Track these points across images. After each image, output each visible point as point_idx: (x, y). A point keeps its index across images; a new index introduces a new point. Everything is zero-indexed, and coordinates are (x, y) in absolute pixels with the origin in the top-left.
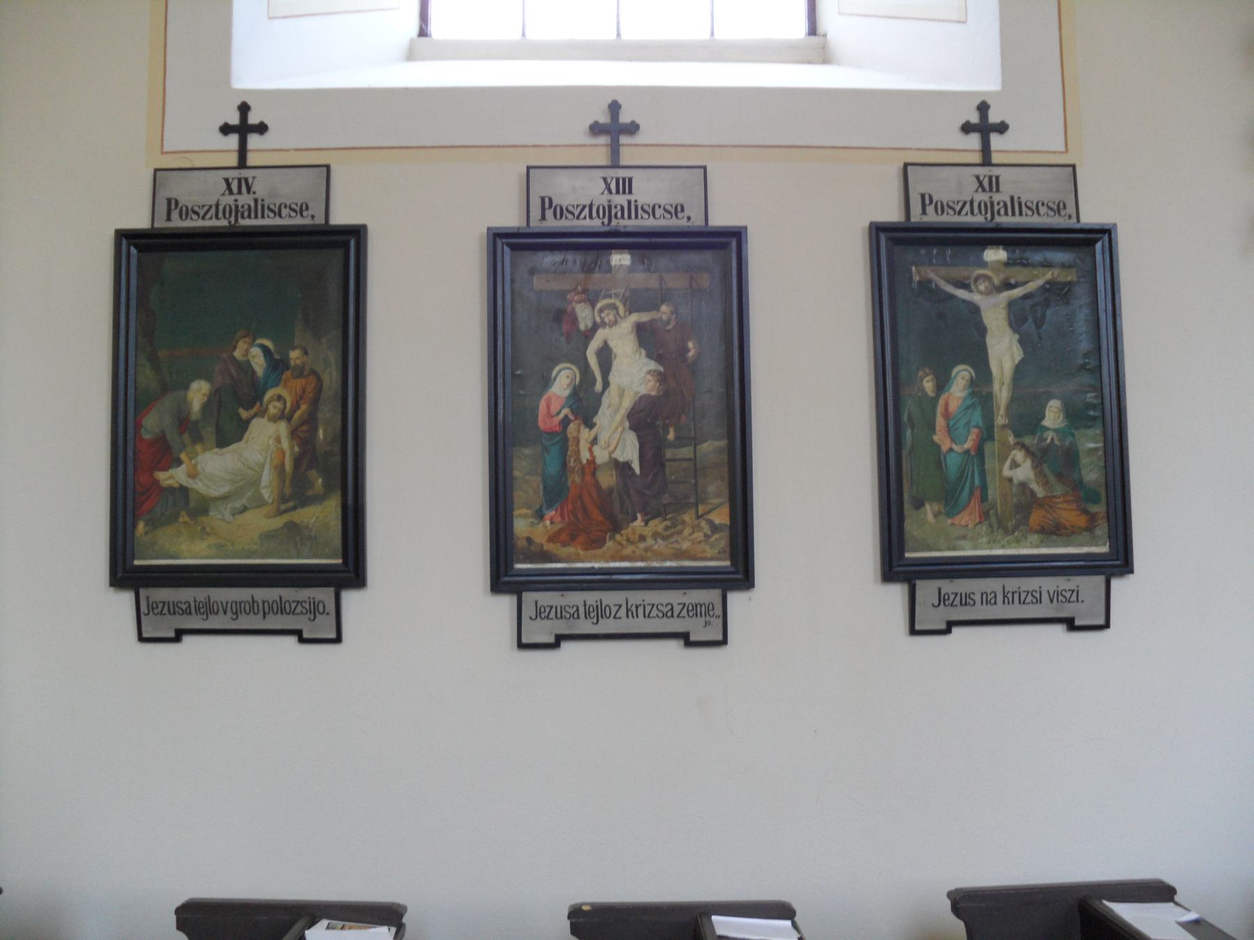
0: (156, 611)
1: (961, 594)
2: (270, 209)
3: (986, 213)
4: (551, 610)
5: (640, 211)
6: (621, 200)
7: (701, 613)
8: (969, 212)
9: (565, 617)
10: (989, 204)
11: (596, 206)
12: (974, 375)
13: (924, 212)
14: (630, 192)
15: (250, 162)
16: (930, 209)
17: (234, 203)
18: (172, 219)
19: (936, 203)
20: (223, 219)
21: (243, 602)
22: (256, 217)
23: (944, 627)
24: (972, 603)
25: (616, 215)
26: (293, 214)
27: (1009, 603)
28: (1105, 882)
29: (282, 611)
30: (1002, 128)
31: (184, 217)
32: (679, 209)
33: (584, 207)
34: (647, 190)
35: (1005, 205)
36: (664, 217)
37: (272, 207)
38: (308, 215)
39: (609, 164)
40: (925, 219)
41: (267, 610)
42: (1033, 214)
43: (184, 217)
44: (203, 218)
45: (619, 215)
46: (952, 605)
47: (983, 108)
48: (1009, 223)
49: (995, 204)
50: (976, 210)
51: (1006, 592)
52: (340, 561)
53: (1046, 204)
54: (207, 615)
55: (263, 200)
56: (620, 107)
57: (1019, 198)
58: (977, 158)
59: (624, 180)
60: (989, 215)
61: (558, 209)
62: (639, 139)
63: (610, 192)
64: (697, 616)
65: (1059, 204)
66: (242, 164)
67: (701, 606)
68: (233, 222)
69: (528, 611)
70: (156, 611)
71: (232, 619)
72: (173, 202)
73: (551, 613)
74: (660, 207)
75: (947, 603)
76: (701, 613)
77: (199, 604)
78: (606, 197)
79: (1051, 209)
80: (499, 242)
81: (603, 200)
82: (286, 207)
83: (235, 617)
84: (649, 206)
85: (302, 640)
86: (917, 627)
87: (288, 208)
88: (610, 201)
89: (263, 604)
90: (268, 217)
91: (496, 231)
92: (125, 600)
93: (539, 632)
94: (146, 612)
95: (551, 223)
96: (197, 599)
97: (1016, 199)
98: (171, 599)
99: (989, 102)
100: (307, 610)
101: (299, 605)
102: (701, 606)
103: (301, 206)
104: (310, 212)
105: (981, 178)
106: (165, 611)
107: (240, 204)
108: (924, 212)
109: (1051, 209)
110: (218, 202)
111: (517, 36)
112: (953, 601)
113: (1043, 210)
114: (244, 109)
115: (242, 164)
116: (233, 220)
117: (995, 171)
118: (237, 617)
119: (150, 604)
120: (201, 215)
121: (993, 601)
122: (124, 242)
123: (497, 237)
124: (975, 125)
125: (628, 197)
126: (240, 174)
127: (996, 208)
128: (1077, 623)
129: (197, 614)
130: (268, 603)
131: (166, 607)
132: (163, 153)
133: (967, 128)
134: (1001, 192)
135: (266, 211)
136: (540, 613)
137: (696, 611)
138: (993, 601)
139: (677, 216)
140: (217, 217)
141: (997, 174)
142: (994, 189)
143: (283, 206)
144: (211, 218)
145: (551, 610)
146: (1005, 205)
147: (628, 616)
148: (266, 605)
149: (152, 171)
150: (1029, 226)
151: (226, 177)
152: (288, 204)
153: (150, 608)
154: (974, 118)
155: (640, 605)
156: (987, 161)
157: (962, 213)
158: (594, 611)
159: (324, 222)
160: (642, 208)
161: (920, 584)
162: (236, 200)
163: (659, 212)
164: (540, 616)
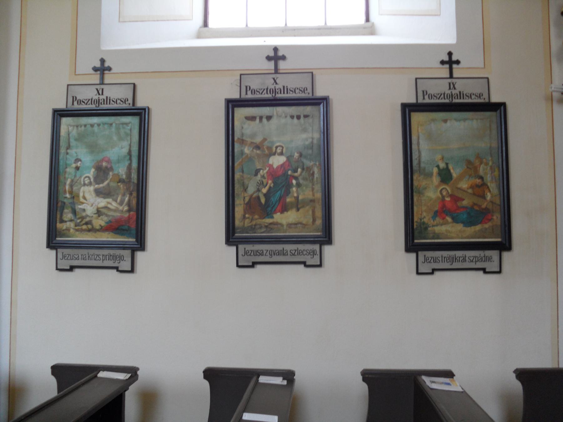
0: (66, 258)
1: (254, 251)
2: (113, 101)
4: (251, 252)
13: (424, 98)
16: (426, 97)
19: (429, 95)
20: (93, 105)
21: (446, 257)
22: (460, 98)
23: (431, 271)
24: (438, 261)
27: (458, 261)
29: (299, 254)
30: (284, 58)
34: (112, 93)
36: (299, 93)
42: (469, 98)
45: (103, 103)
46: (250, 255)
51: (456, 257)
54: (313, 256)
57: (110, 97)
58: (273, 72)
62: (460, 66)
63: (99, 94)
71: (270, 257)
72: (425, 92)
74: (119, 99)
75: (248, 254)
77: (299, 251)
78: (98, 96)
79: (300, 90)
81: (96, 97)
82: (473, 94)
83: (271, 256)
84: (123, 99)
85: (118, 271)
87: (474, 95)
88: (99, 97)
89: (280, 251)
96: (443, 256)
97: (461, 93)
101: (472, 260)
102: (476, 257)
105: (99, 90)
109: (477, 96)
110: (445, 92)
111: (322, 24)
112: (431, 260)
114: (103, 61)
117: (454, 81)
118: (272, 257)
121: (286, 254)
138: (286, 254)
144: (89, 104)
145: (251, 252)
146: (457, 95)
151: (97, 88)
152: (474, 94)
153: (426, 260)
157: (88, 104)
160: (466, 94)
161: (420, 253)
163: (297, 91)
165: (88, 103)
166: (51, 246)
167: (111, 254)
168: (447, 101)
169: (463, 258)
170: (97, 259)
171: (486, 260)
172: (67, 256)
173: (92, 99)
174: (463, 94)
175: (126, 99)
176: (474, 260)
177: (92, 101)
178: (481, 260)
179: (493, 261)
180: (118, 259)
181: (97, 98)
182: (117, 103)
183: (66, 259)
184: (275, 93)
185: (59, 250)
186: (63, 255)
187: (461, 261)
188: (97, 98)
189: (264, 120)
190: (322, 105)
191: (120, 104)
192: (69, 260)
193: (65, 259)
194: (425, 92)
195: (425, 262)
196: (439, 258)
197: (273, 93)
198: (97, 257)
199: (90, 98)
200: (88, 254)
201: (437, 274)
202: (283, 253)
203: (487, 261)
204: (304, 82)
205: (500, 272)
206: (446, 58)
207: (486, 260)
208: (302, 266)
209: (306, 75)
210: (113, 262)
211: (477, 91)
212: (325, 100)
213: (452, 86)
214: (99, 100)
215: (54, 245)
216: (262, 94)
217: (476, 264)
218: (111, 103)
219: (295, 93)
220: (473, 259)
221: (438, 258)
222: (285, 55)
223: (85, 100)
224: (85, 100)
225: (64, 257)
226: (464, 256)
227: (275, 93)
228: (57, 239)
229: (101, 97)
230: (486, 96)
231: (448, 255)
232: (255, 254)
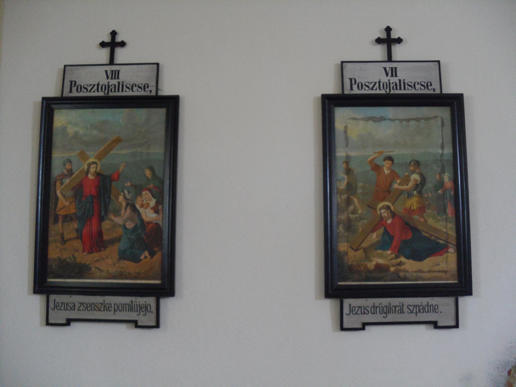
0: (58, 308)
3: (387, 88)
5: (125, 88)
6: (115, 82)
7: (137, 307)
9: (96, 309)
10: (388, 84)
12: (449, 175)
13: (352, 89)
14: (118, 78)
16: (355, 87)
17: (388, 81)
18: (72, 91)
20: (383, 90)
23: (360, 326)
25: (393, 87)
32: (429, 84)
33: (94, 85)
35: (115, 86)
38: (432, 89)
40: (353, 92)
44: (372, 89)
45: (113, 90)
49: (391, 83)
53: (419, 83)
55: (123, 82)
57: (404, 80)
60: (106, 91)
61: (79, 87)
64: (92, 310)
65: (145, 84)
67: (126, 305)
68: (388, 92)
69: (346, 310)
70: (354, 312)
72: (73, 83)
73: (359, 311)
76: (137, 307)
82: (418, 84)
85: (137, 326)
92: (38, 301)
94: (53, 308)
95: (356, 91)
97: (402, 81)
98: (91, 302)
102: (126, 305)
104: (433, 87)
106: (63, 308)
107: (110, 84)
108: (352, 89)
112: (358, 311)
113: (417, 87)
116: (388, 90)
117: (393, 65)
122: (327, 101)
125: (118, 80)
127: (392, 86)
130: (117, 305)
131: (63, 305)
134: (70, 81)
137: (92, 307)
141: (395, 66)
142: (394, 75)
143: (134, 85)
148: (116, 306)
151: (106, 70)
152: (137, 85)
153: (140, 308)
154: (384, 36)
155: (378, 307)
156: (112, 62)
162: (389, 80)
164: (352, 313)
165: (374, 88)
167: (376, 305)
168: (101, 94)
169: (400, 307)
172: (357, 309)
173: (379, 82)
174: (404, 83)
175: (146, 85)
179: (439, 312)
180: (143, 310)
181: (106, 84)
183: (90, 311)
187: (397, 312)
188: (106, 84)
191: (138, 91)
192: (62, 310)
193: (57, 309)
194: (73, 83)
195: (54, 308)
196: (368, 307)
197: (387, 88)
198: (101, 308)
200: (390, 306)
201: (73, 324)
203: (430, 312)
205: (457, 326)
206: (384, 36)
207: (429, 311)
210: (137, 315)
211: (141, 81)
213: (116, 75)
214: (109, 85)
216: (90, 92)
217: (416, 315)
218: (124, 90)
224: (369, 83)
225: (351, 310)
226: (401, 304)
228: (49, 280)
230: (436, 85)
231: (400, 303)
232: (66, 308)
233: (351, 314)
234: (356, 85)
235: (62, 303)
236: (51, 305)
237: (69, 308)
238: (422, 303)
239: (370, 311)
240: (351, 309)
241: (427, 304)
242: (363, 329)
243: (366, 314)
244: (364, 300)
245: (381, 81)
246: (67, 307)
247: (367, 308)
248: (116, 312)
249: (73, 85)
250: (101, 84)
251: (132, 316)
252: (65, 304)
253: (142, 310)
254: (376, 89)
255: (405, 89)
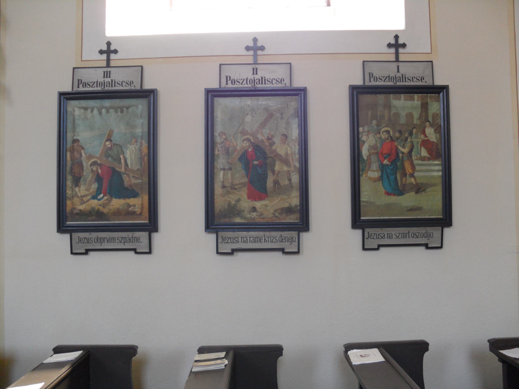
0: (82, 242)
2: (118, 84)
6: (109, 80)
8: (388, 80)
10: (395, 78)
11: (249, 79)
15: (112, 65)
16: (229, 82)
20: (99, 87)
23: (376, 247)
24: (91, 242)
26: (127, 85)
28: (266, 345)
30: (115, 52)
31: (84, 87)
32: (132, 83)
34: (117, 75)
35: (259, 80)
36: (276, 84)
37: (269, 80)
39: (252, 62)
40: (227, 86)
41: (132, 239)
43: (84, 87)
47: (397, 37)
48: (92, 90)
50: (248, 83)
52: (148, 222)
53: (125, 82)
56: (398, 37)
59: (107, 72)
60: (253, 84)
62: (407, 50)
65: (131, 82)
66: (108, 66)
67: (114, 238)
70: (82, 242)
74: (124, 82)
79: (127, 83)
80: (62, 97)
82: (415, 78)
85: (136, 253)
86: (366, 247)
89: (256, 238)
90: (267, 84)
91: (208, 90)
93: (226, 248)
95: (230, 86)
99: (111, 42)
100: (237, 241)
101: (398, 236)
103: (281, 80)
107: (106, 81)
108: (227, 84)
114: (109, 44)
115: (108, 66)
119: (80, 239)
120: (241, 82)
123: (62, 95)
124: (256, 45)
126: (398, 64)
127: (397, 79)
128: (429, 246)
129: (259, 242)
130: (424, 237)
132: (82, 61)
133: (390, 45)
135: (266, 82)
136: (80, 240)
139: (413, 81)
140: (389, 81)
141: (256, 67)
144: (387, 82)
147: (265, 242)
149: (362, 62)
150: (274, 89)
154: (393, 42)
158: (284, 239)
159: (432, 84)
161: (73, 234)
163: (124, 84)
165: (93, 86)
166: (63, 230)
170: (273, 241)
171: (134, 241)
172: (373, 235)
175: (282, 80)
176: (123, 241)
177: (389, 78)
178: (130, 240)
181: (394, 76)
182: (122, 86)
184: (104, 85)
185: (73, 234)
186: (79, 239)
189: (125, 109)
190: (441, 94)
195: (222, 242)
197: (102, 86)
199: (96, 81)
202: (111, 240)
204: (280, 73)
206: (393, 42)
207: (134, 241)
208: (280, 254)
209: (286, 65)
212: (444, 89)
213: (107, 75)
215: (65, 228)
216: (384, 81)
217: (124, 245)
218: (116, 86)
219: (413, 81)
220: (399, 235)
221: (276, 238)
222: (406, 43)
223: (382, 77)
224: (90, 82)
227: (104, 85)
228: (67, 223)
229: (256, 77)
233: (369, 238)
234: (373, 78)
235: (85, 238)
236: (366, 235)
237: (416, 237)
238: (128, 235)
239: (94, 241)
240: (369, 235)
241: (132, 236)
242: (377, 249)
243: (91, 243)
244: (379, 229)
245: (390, 76)
246: (378, 236)
247: (91, 239)
248: (125, 244)
249: (80, 83)
250: (249, 78)
251: (423, 241)
252: (377, 235)
253: (138, 241)
254: (244, 84)
255: (265, 84)
